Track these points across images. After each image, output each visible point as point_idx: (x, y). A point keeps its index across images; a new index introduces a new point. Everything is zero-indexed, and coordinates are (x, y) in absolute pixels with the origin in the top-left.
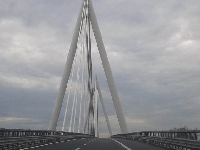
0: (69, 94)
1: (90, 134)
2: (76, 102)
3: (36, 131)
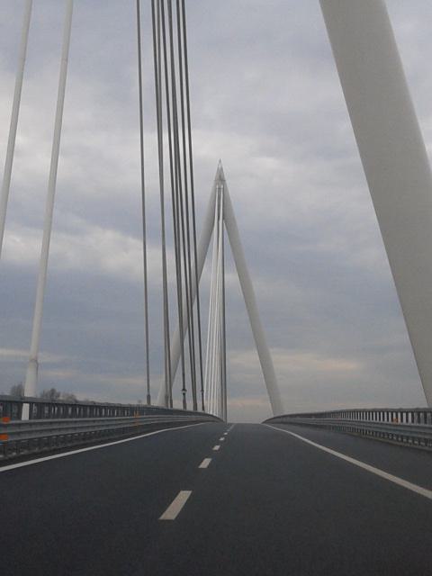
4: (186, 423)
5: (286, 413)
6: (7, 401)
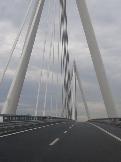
0: (47, 85)
1: (65, 117)
4: (60, 122)
5: (92, 119)
6: (8, 116)
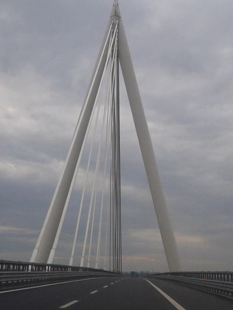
1: (112, 270)
2: (94, 209)
3: (25, 265)
4: (100, 276)
